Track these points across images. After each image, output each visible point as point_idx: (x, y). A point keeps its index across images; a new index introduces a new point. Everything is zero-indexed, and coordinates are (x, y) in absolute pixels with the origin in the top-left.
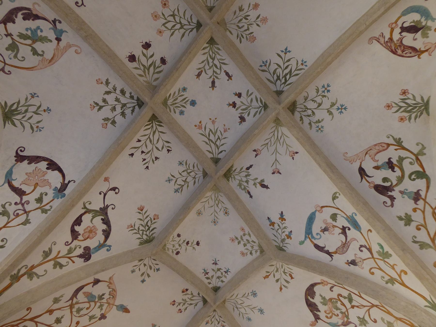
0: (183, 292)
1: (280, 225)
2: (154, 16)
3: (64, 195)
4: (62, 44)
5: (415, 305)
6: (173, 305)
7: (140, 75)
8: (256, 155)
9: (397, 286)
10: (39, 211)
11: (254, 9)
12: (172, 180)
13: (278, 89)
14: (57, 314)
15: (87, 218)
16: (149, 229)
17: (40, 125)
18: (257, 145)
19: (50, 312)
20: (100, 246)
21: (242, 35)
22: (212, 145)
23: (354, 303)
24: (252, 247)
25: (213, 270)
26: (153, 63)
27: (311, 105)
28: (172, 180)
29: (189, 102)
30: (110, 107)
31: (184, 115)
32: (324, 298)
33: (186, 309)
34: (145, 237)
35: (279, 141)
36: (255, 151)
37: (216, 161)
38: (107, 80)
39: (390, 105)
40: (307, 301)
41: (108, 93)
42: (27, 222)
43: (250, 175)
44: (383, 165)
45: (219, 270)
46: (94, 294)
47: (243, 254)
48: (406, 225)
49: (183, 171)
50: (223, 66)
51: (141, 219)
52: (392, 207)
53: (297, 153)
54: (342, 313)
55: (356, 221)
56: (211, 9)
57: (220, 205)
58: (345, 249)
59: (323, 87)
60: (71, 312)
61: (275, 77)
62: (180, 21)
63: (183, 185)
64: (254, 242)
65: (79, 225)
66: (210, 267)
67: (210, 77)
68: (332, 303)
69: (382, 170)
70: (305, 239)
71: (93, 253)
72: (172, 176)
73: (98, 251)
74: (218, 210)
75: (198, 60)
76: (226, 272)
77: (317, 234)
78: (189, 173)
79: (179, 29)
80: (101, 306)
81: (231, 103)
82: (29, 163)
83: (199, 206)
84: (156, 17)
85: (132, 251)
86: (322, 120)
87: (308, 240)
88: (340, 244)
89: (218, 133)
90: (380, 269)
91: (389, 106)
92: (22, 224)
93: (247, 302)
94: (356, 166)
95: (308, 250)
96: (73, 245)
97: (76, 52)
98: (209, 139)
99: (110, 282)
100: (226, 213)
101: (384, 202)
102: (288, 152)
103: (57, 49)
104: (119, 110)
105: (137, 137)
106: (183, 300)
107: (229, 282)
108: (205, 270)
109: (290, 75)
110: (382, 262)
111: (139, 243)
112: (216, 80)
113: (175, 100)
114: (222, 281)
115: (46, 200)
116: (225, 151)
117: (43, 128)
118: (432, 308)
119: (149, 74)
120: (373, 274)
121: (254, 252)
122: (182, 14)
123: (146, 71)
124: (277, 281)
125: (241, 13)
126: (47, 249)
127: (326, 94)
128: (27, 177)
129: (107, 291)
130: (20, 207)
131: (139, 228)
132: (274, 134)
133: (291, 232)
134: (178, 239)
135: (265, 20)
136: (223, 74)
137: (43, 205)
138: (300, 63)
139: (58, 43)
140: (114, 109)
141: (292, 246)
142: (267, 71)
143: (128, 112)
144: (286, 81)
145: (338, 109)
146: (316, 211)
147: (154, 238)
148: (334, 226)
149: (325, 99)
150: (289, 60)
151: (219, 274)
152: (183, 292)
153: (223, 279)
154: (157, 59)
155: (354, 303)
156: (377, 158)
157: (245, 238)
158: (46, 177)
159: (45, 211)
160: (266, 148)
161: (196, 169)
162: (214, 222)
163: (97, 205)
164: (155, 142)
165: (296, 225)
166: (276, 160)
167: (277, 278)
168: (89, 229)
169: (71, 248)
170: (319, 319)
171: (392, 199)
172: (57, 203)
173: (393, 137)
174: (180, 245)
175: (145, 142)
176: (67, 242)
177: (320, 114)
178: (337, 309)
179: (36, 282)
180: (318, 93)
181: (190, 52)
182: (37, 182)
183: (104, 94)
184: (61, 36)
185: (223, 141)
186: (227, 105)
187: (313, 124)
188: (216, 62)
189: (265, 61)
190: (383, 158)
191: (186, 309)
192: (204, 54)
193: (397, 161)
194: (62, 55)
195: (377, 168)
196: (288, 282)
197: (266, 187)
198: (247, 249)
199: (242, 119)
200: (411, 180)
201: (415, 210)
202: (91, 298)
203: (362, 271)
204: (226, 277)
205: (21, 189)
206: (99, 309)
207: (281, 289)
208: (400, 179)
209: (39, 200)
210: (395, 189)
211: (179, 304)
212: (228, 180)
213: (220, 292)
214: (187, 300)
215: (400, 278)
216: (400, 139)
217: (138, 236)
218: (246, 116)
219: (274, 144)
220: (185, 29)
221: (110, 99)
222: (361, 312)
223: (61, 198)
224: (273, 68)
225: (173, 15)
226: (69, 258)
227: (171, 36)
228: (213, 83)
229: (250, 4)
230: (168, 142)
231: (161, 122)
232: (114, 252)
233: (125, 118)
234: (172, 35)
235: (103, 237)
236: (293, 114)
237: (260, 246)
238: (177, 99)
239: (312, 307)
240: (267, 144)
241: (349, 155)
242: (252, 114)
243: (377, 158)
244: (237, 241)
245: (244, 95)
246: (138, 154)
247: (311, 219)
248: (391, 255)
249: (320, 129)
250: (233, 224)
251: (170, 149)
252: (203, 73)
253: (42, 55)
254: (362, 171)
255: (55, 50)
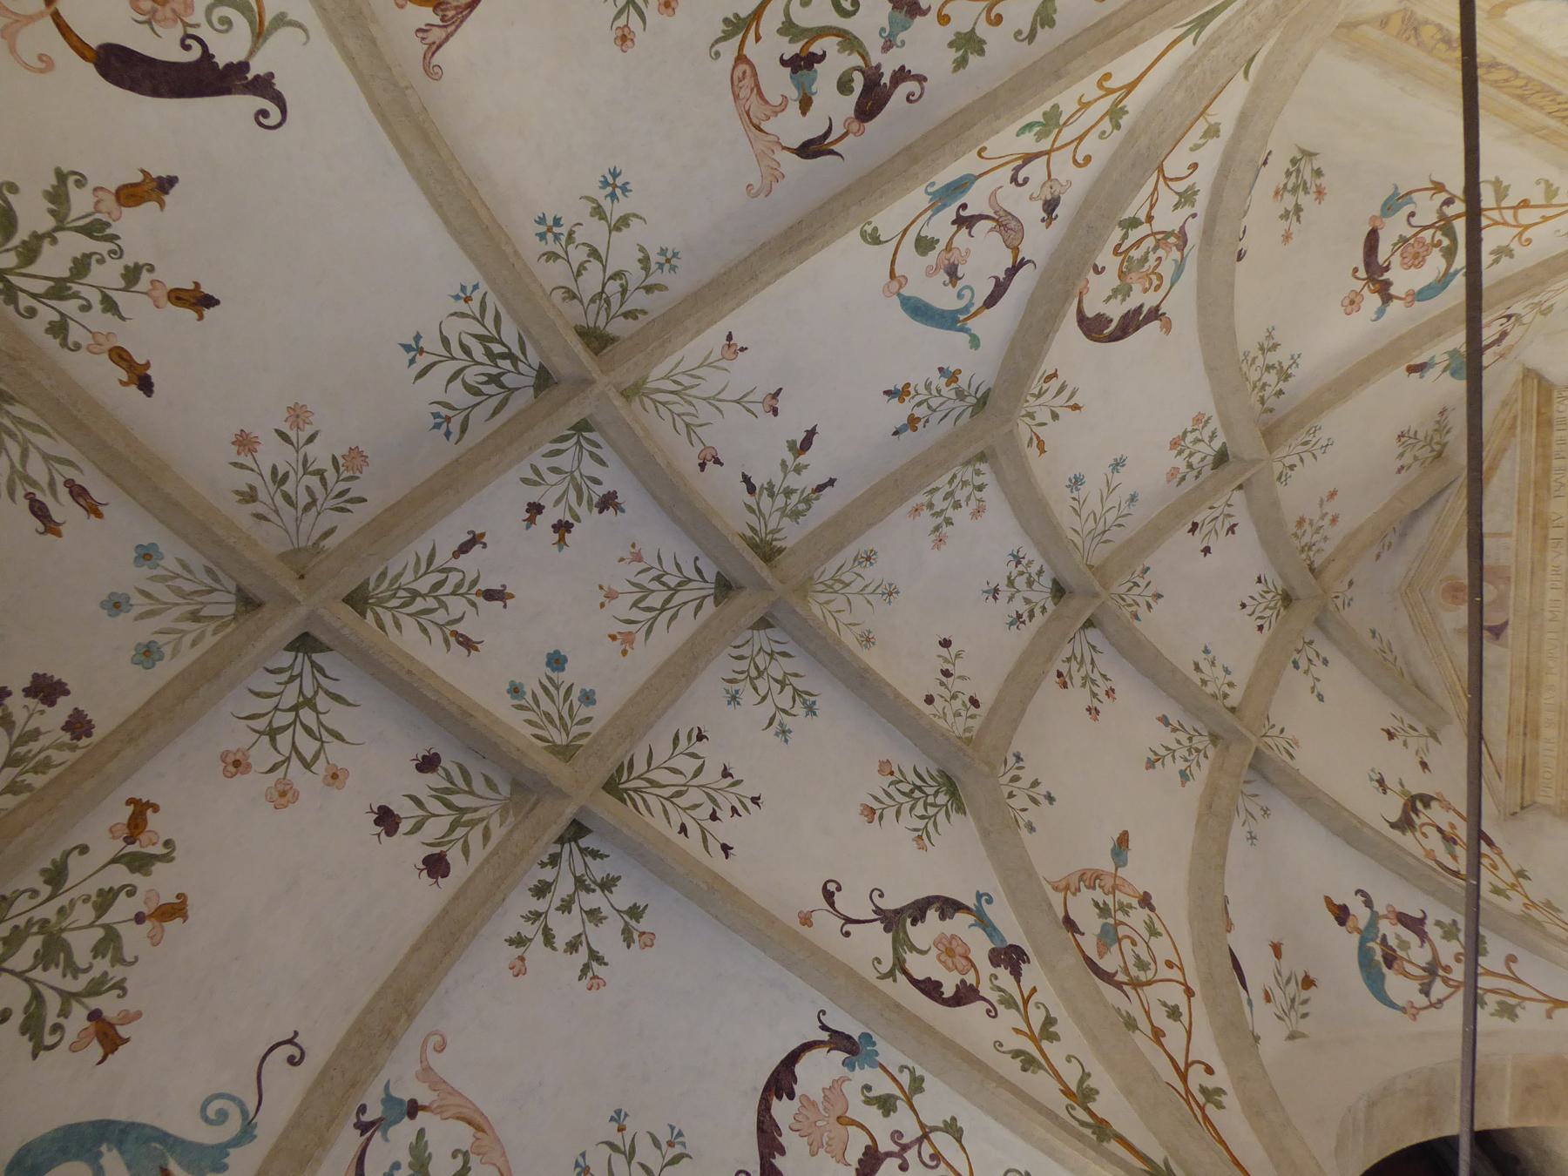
0: (1065, 686)
1: (918, 399)
2: (283, 801)
3: (866, 1037)
4: (424, 1096)
5: (1188, 67)
6: (1098, 712)
7: (486, 836)
8: (717, 461)
9: (1131, 103)
10: (916, 1099)
11: (252, 451)
12: (781, 724)
13: (531, 381)
14: (1161, 1019)
15: (922, 967)
16: (919, 788)
17: (664, 1137)
18: (686, 457)
19: (1158, 1034)
20: (983, 922)
21: (338, 496)
22: (679, 598)
23: (1142, 216)
24: (965, 483)
25: (1011, 599)
26: (441, 795)
27: (591, 282)
28: (781, 724)
29: (554, 675)
30: (590, 927)
31: (593, 692)
32: (1115, 292)
33: (1104, 676)
34: (942, 799)
35: (686, 388)
36: (702, 466)
37: (725, 588)
38: (511, 942)
39: (620, 33)
40: (1113, 338)
41: (549, 938)
42: (953, 1129)
43: (770, 483)
44: (800, 86)
45: (1011, 583)
46: (1098, 931)
47: (978, 512)
48: (981, 52)
49: (755, 689)
50: (437, 563)
51: (898, 813)
52: (925, 79)
53: (730, 337)
54: (1155, 249)
55: (949, 185)
56: (248, 603)
57: (846, 578)
58: (1013, 224)
59: (542, 236)
60: (1149, 983)
61: (491, 389)
62: (290, 710)
63: (795, 689)
64: (954, 476)
65: (938, 985)
66: (1004, 609)
67: (473, 604)
68: (1130, 271)
69: (814, 89)
70: (966, 331)
71: (1003, 940)
72: (770, 724)
73: (995, 929)
74: (858, 584)
75: (413, 643)
76: (1018, 563)
77: (960, 296)
78: (760, 674)
79: (318, 713)
80: (1125, 909)
81: (556, 537)
82: (782, 1152)
83: (850, 639)
84: (284, 795)
85: (985, 834)
86: (642, 249)
87: (970, 324)
88: (997, 237)
89: (644, 579)
90: (1081, 138)
91: (624, 38)
92: (959, 1140)
93: (1094, 504)
94: (791, 163)
95: (996, 325)
96: (993, 997)
97: (441, 1049)
98: (663, 610)
99: (1065, 888)
100: (868, 559)
101: (908, 99)
102: (723, 363)
103: (439, 1110)
104: (594, 900)
105: (673, 834)
106: (1084, 685)
107: (1044, 554)
108: (1011, 624)
109: (493, 340)
110: (1065, 130)
111: (960, 816)
112: (482, 586)
113: (552, 721)
114: (1040, 573)
115: (884, 1087)
116: (697, 559)
117: (673, 1128)
118: (1204, 27)
119: (476, 810)
120: (1088, 159)
121: (978, 481)
122: (268, 704)
123: (466, 817)
124: (1055, 416)
125: (262, 494)
126: (1017, 1063)
127: (564, 230)
128: (822, 1152)
129: (1087, 895)
130: (911, 1155)
131: (922, 817)
132: (664, 404)
133: (941, 369)
134: (938, 702)
135: (297, 414)
136: (463, 561)
137: (898, 1093)
138: (461, 306)
139: (424, 1108)
140: (594, 915)
141: (980, 369)
142: (467, 417)
143: (599, 870)
144: (509, 356)
145: (613, 196)
146: (899, 295)
147: (942, 773)
148: (949, 248)
149: (579, 237)
150: (445, 341)
151: (1021, 582)
152: (1065, 686)
153: (1034, 570)
154: (423, 784)
155: (1142, 216)
156: (775, 99)
157: (939, 504)
158: (817, 1096)
159: (917, 1084)
160: (698, 430)
161: (745, 651)
162: (890, 594)
163: (877, 940)
164: (680, 779)
165: (923, 354)
166: (738, 402)
167: (1047, 418)
168: (943, 957)
169: (1001, 1002)
170: (1157, 308)
171: (901, 75)
172: (888, 1053)
173: (717, 41)
174: (954, 697)
175: (684, 809)
176: (988, 1012)
177: (622, 255)
178: (1145, 259)
179: (1100, 1079)
180: (558, 256)
181: (409, 672)
182: (833, 1120)
183: (554, 949)
184: (401, 1101)
185: (669, 566)
186: (560, 549)
187: (650, 281)
188: (424, 585)
189: (432, 421)
190: (778, 83)
191: (1104, 676)
192: (398, 626)
193: (791, 41)
194: (454, 1092)
195: (805, 104)
196: (1062, 388)
197: (811, 433)
198: (968, 498)
199: (608, 502)
200: (854, 13)
201: (944, 19)
202: (1109, 937)
203: (1075, 183)
204: (1030, 562)
205: (860, 1161)
206: (1131, 912)
207: (1076, 407)
208: (850, 42)
209: (886, 1105)
210: (874, 64)
211: (1094, 695)
212: (780, 551)
213: (1070, 580)
214: (1083, 673)
215: (1113, 91)
216: (726, 21)
217: (941, 817)
218: (601, 491)
219: (691, 404)
220: (316, 693)
221: (565, 927)
222: (1167, 198)
223: (874, 1044)
224: (458, 395)
225: (272, 733)
226: (1026, 1002)
227: (343, 740)
228: (490, 595)
229: (235, 464)
230: (676, 738)
231: (622, 766)
232: (993, 885)
233: (619, 878)
234: (337, 736)
235: (959, 916)
236: (613, 340)
237: (967, 463)
238: (547, 715)
239: (1130, 324)
240: (687, 425)
241: (755, 180)
242: (590, 468)
243: (775, 99)
244: (945, 529)
245: (534, 494)
246: (725, 830)
247: (919, 310)
248: (1056, 107)
249: (668, 261)
250: (899, 539)
251: (695, 732)
252: (461, 628)
253: (466, 1154)
254: (810, 149)
255: (446, 1115)
